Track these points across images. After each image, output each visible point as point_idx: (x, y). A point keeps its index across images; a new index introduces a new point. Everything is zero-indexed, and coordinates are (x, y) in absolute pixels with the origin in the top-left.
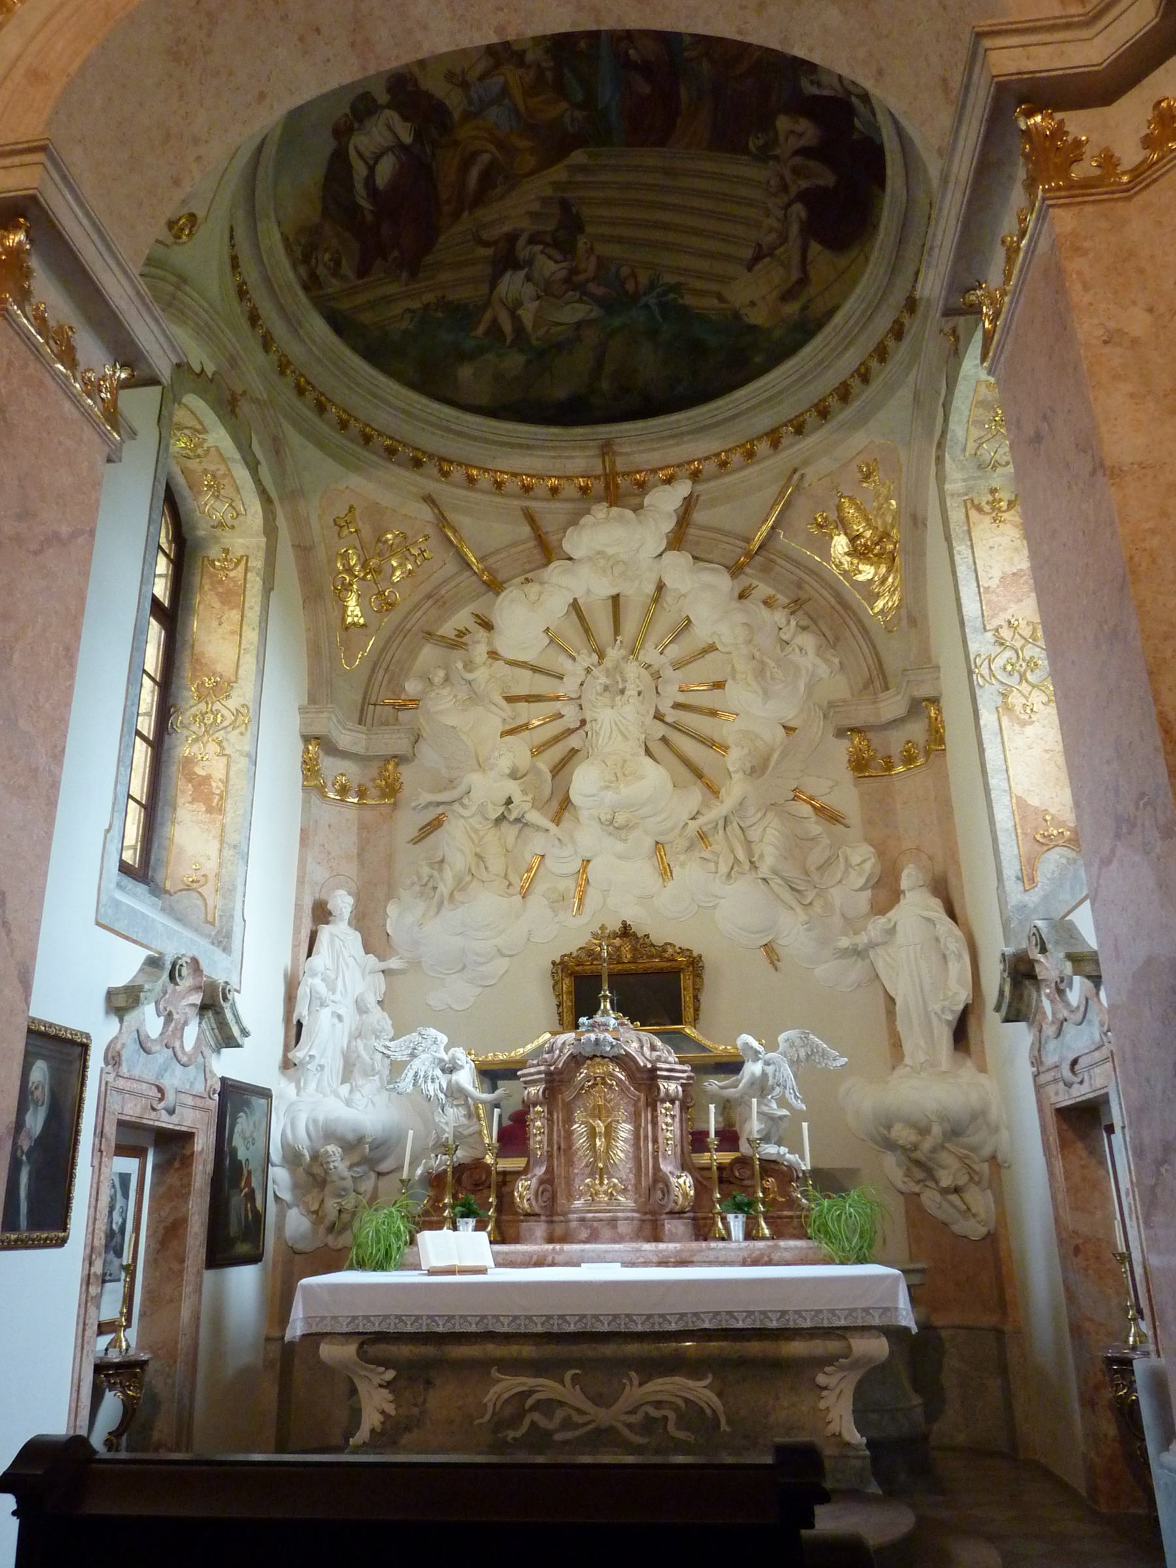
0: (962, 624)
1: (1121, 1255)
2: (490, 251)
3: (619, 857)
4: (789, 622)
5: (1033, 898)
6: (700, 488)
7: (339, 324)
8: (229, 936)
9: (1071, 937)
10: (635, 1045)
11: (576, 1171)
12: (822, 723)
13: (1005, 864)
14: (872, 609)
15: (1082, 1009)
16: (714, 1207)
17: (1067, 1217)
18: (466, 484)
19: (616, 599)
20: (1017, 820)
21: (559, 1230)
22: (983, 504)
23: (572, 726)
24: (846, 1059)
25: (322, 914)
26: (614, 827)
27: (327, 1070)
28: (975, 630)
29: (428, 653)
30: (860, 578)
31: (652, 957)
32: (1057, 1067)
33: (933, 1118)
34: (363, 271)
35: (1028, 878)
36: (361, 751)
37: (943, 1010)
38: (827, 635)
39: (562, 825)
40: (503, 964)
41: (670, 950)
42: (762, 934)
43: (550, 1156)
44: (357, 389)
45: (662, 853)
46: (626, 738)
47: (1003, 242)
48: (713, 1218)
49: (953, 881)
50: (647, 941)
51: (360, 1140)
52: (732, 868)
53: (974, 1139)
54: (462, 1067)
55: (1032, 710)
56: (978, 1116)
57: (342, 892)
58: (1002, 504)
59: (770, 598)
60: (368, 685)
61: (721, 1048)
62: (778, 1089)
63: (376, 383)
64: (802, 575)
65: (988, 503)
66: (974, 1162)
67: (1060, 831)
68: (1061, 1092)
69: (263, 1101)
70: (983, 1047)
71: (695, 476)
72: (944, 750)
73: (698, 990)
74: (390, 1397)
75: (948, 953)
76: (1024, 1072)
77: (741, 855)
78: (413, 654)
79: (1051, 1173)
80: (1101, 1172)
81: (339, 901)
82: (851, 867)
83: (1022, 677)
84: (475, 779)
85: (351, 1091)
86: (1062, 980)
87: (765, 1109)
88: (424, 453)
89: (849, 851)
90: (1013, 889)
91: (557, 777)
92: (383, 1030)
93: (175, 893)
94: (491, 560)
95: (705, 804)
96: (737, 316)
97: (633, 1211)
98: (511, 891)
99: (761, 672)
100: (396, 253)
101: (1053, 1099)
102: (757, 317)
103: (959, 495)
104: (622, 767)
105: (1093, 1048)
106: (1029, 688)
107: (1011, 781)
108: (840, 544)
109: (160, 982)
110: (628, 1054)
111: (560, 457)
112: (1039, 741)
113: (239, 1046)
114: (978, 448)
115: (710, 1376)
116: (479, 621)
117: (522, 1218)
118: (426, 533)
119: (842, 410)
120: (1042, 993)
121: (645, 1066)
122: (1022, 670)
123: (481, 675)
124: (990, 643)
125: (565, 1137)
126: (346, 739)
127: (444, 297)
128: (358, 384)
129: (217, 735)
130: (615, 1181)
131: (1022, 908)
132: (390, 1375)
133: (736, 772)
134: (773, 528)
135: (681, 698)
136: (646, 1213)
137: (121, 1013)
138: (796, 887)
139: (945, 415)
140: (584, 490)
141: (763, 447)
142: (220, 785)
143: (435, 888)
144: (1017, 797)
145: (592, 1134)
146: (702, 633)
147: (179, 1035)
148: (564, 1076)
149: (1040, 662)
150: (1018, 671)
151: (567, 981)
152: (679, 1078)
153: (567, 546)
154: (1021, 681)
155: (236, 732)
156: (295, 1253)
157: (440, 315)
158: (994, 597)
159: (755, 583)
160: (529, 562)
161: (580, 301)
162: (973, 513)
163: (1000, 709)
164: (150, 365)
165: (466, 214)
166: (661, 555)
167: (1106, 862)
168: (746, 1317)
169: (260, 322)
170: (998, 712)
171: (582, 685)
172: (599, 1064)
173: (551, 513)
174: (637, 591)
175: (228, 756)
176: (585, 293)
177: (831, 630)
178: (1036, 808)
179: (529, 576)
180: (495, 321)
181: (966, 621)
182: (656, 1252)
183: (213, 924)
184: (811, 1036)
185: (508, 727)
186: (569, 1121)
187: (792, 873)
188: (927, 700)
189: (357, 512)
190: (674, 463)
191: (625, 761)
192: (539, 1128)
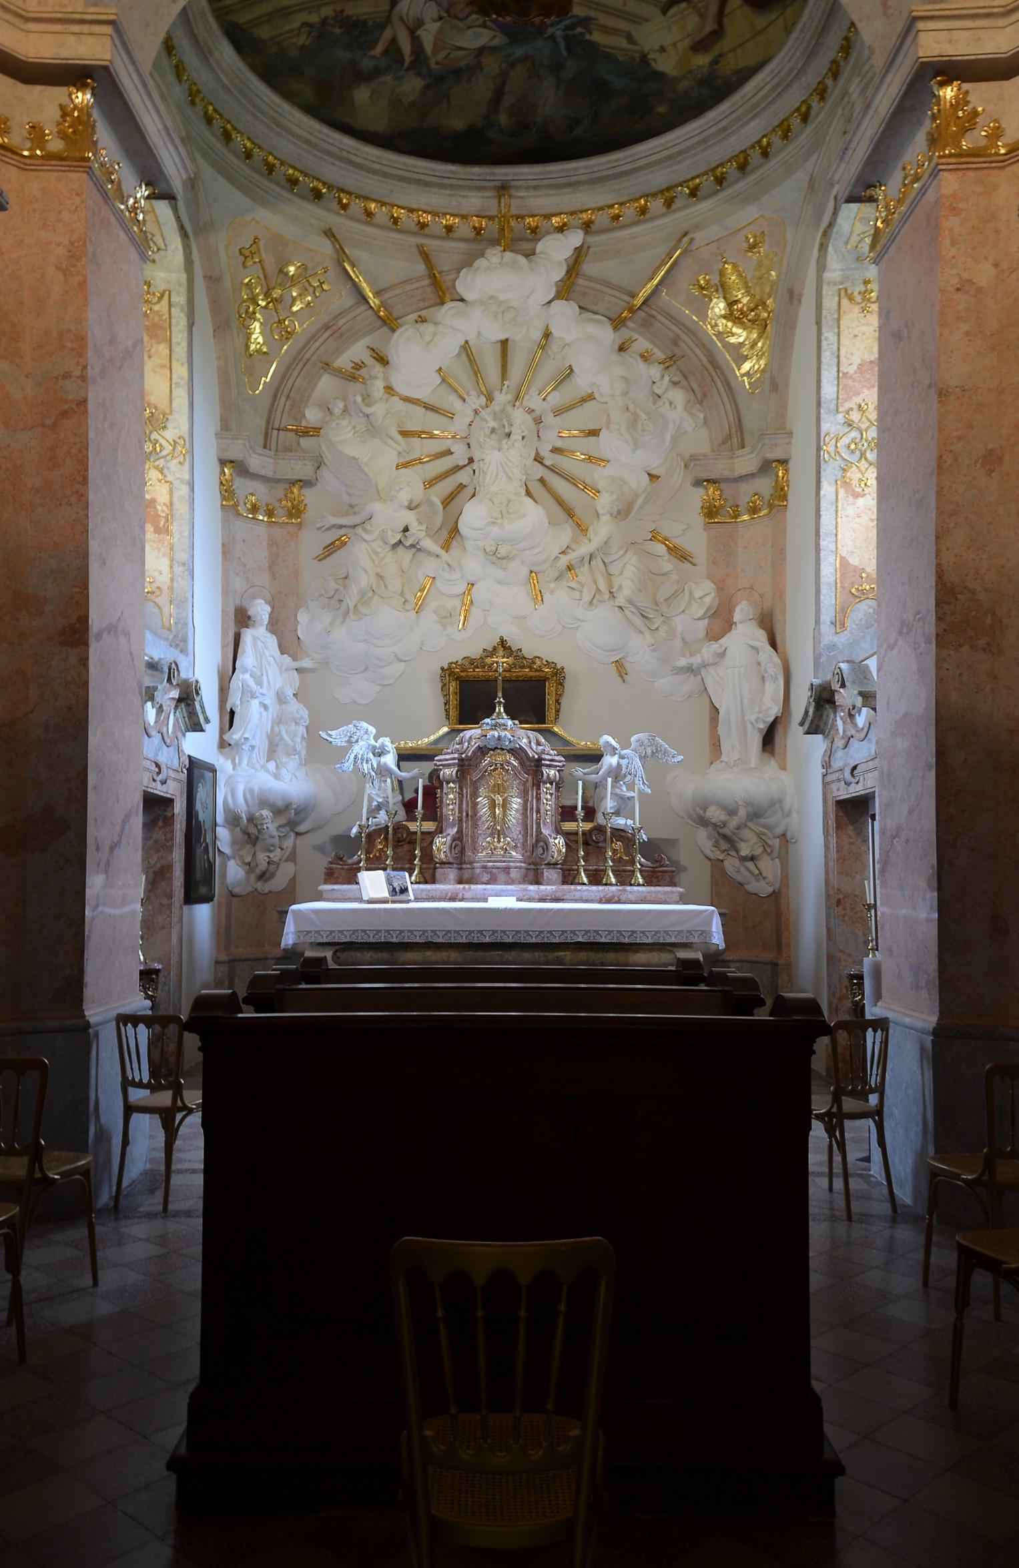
0: (819, 404)
1: (869, 905)
3: (500, 582)
5: (842, 639)
6: (592, 239)
8: (184, 640)
9: (865, 678)
10: (525, 740)
11: (480, 832)
12: (682, 473)
13: (823, 610)
15: (866, 730)
16: (579, 861)
17: (834, 879)
19: (504, 343)
20: (838, 576)
21: (467, 875)
22: (856, 294)
23: (461, 463)
24: (682, 757)
25: (243, 619)
26: (496, 557)
27: (256, 750)
28: (829, 411)
29: (326, 384)
30: (732, 340)
31: (523, 667)
33: (740, 803)
36: (270, 474)
37: (757, 719)
38: (695, 391)
40: (399, 667)
41: (538, 662)
42: (615, 653)
43: (460, 820)
44: (262, 117)
45: (535, 582)
46: (510, 479)
47: (904, 169)
48: (578, 870)
49: (778, 617)
50: (519, 653)
51: (287, 807)
53: (770, 821)
54: (389, 752)
55: (866, 484)
56: (776, 803)
57: (260, 601)
58: (872, 294)
59: (647, 351)
60: (270, 410)
61: (583, 743)
62: (629, 777)
63: (280, 111)
64: (679, 332)
66: (769, 838)
67: (872, 586)
68: (841, 789)
69: (211, 774)
70: (785, 750)
71: (587, 227)
72: (786, 506)
73: (560, 695)
75: (766, 675)
76: (817, 771)
77: (602, 586)
78: (313, 383)
79: (827, 846)
80: (864, 848)
81: (259, 609)
82: (695, 600)
84: (377, 507)
85: (277, 767)
86: (854, 708)
87: (618, 791)
90: (826, 629)
91: (447, 507)
92: (302, 718)
94: (386, 296)
95: (575, 540)
96: (644, 59)
97: (521, 862)
98: (407, 606)
99: (633, 424)
102: (666, 65)
103: (835, 284)
104: (507, 505)
106: (867, 466)
107: (839, 543)
108: (719, 307)
111: (455, 195)
112: (867, 511)
113: (202, 730)
114: (860, 242)
116: (375, 355)
118: (325, 265)
120: (838, 714)
122: (863, 448)
123: (378, 410)
124: (840, 424)
126: (258, 462)
127: (342, 11)
128: (263, 113)
129: (157, 463)
130: (509, 839)
131: (832, 647)
133: (603, 515)
134: (657, 286)
135: (559, 444)
136: (530, 864)
138: (646, 614)
139: (835, 209)
140: (478, 231)
141: (657, 205)
143: (340, 601)
144: (841, 556)
145: (493, 805)
146: (582, 382)
147: (166, 723)
148: (472, 762)
150: (860, 450)
151: (453, 683)
152: (557, 766)
153: (461, 287)
154: (861, 458)
155: (175, 462)
157: (337, 30)
158: (850, 383)
160: (424, 300)
161: (484, 26)
162: (845, 302)
163: (838, 482)
167: (891, 647)
168: (608, 935)
169: (174, 52)
170: (837, 484)
172: (499, 754)
173: (446, 252)
174: (525, 337)
175: (171, 483)
177: (700, 386)
178: (856, 566)
179: (423, 313)
180: (394, 41)
182: (537, 892)
183: (170, 630)
185: (403, 460)
186: (475, 794)
189: (261, 243)
190: (567, 210)
191: (509, 501)
192: (452, 799)
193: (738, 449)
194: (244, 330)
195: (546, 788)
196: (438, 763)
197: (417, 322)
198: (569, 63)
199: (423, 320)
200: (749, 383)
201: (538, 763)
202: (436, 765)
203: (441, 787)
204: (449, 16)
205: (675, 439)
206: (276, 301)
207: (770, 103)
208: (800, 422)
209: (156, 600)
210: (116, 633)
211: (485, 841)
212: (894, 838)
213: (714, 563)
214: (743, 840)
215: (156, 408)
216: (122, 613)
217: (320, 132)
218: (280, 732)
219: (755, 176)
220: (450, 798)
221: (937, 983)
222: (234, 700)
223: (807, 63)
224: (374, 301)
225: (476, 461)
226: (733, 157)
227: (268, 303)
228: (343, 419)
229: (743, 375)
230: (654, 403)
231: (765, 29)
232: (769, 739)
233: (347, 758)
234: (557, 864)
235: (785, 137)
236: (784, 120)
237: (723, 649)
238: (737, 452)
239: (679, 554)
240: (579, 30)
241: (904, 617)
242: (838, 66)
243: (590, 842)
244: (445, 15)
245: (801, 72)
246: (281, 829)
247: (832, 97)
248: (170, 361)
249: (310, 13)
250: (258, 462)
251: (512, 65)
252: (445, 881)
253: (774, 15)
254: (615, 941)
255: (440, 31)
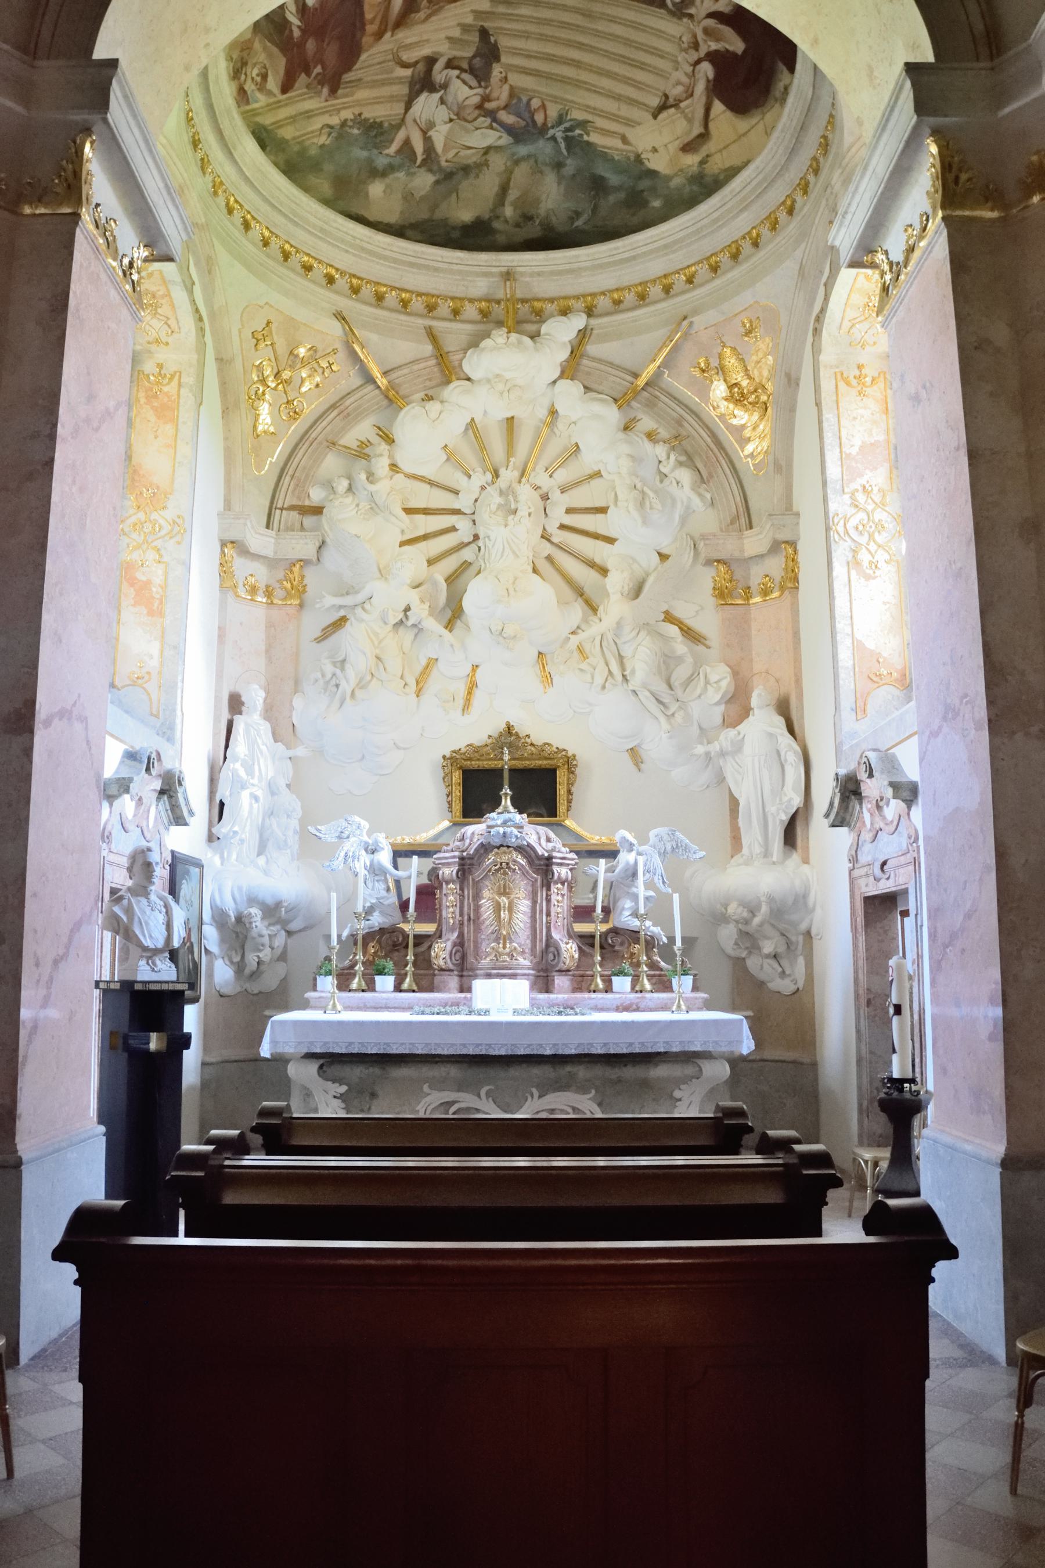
0: (825, 483)
2: (408, 72)
4: (668, 458)
6: (594, 322)
7: (264, 138)
8: (172, 728)
9: (893, 767)
11: (483, 937)
14: (743, 451)
15: (895, 823)
18: (373, 301)
19: (511, 420)
22: (851, 378)
23: (466, 540)
24: (704, 853)
25: (236, 704)
30: (735, 422)
32: (869, 865)
33: (763, 899)
34: (285, 88)
35: (860, 709)
36: (271, 554)
38: (702, 471)
39: (456, 631)
43: (461, 924)
50: (528, 740)
51: (278, 905)
52: (606, 680)
54: (383, 849)
55: (876, 566)
61: (595, 838)
63: (298, 202)
65: (855, 377)
69: (197, 870)
71: (590, 312)
73: (572, 784)
74: (343, 1105)
83: (871, 537)
85: (267, 862)
86: (882, 800)
88: (337, 270)
89: (708, 669)
93: (123, 687)
94: (393, 375)
95: (585, 620)
96: (638, 159)
97: (529, 969)
98: (407, 689)
100: (318, 69)
101: (864, 889)
102: (658, 163)
103: (831, 367)
104: (514, 583)
105: (900, 854)
106: (875, 547)
108: (719, 389)
109: (141, 775)
110: (529, 845)
113: (186, 824)
114: (851, 327)
115: (593, 1092)
116: (381, 433)
117: (436, 972)
119: (732, 268)
121: (543, 855)
122: (871, 530)
125: (474, 910)
127: (360, 115)
129: (155, 544)
130: (516, 945)
132: (343, 1089)
137: (111, 799)
139: (826, 295)
142: (160, 590)
143: (337, 686)
145: (498, 908)
146: (589, 460)
147: (146, 816)
149: (886, 525)
150: (868, 532)
152: (569, 865)
153: (467, 368)
156: (221, 996)
157: (356, 131)
159: (640, 416)
160: (430, 380)
161: (491, 127)
162: (842, 385)
164: (168, 246)
165: (388, 34)
166: (555, 382)
167: (934, 734)
169: (200, 146)
171: (476, 500)
172: (505, 853)
173: (454, 333)
174: (530, 416)
176: (495, 120)
177: (705, 466)
179: (430, 393)
180: (407, 142)
181: (828, 483)
183: (157, 716)
184: (677, 833)
186: (477, 896)
187: (661, 688)
188: (786, 542)
189: (273, 326)
191: (516, 579)
192: (452, 902)
193: (747, 530)
194: (254, 411)
195: (557, 888)
196: (437, 862)
197: (423, 400)
198: (569, 161)
199: (430, 398)
200: (753, 465)
201: (548, 861)
202: (434, 863)
203: (440, 887)
204: (459, 118)
205: (684, 520)
206: (288, 382)
207: (757, 197)
208: (805, 499)
209: (144, 685)
210: (69, 719)
211: (488, 946)
212: (947, 947)
213: (728, 645)
214: (768, 938)
215: (158, 488)
216: (79, 696)
217: (335, 221)
218: (271, 825)
219: (748, 264)
220: (449, 898)
221: (1004, 1109)
222: (223, 792)
223: (789, 160)
224: (382, 382)
225: (481, 537)
226: (725, 247)
227: (278, 384)
228: (347, 497)
229: (746, 457)
230: (661, 481)
231: (746, 133)
232: (790, 835)
233: (337, 856)
234: (569, 971)
235: (773, 228)
236: (770, 213)
237: (741, 736)
238: (746, 532)
239: (690, 634)
240: (578, 132)
241: (949, 701)
242: (818, 162)
243: (605, 946)
244: (455, 117)
245: (785, 167)
246: (272, 928)
247: (815, 190)
248: (176, 441)
249: (331, 115)
250: (261, 541)
251: (517, 162)
252: (449, 991)
253: (754, 121)
254: (483, 1052)
255: (451, 130)
